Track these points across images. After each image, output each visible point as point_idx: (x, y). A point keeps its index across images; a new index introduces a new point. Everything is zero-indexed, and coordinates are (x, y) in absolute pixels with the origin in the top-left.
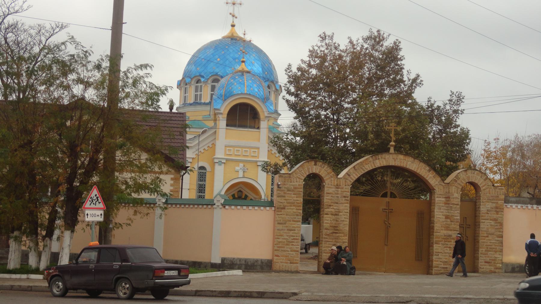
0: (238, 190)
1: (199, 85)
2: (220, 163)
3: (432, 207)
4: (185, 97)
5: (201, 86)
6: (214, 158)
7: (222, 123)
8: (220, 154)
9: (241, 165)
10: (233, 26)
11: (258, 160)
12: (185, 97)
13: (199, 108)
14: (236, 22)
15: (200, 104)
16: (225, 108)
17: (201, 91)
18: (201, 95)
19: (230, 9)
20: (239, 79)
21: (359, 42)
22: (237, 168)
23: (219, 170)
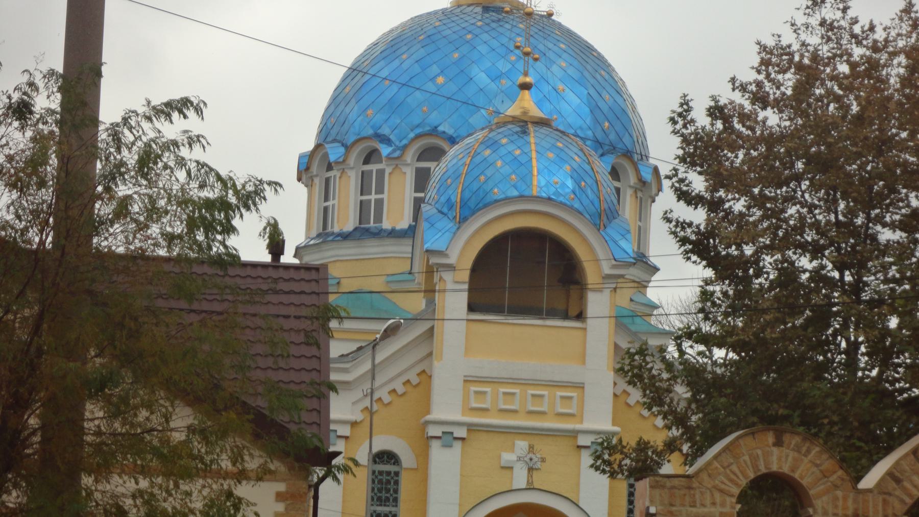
1: (373, 167)
2: (448, 439)
4: (326, 210)
5: (381, 173)
6: (428, 423)
7: (455, 301)
8: (447, 407)
11: (578, 427)
12: (326, 210)
13: (372, 248)
16: (462, 247)
17: (380, 190)
18: (379, 203)
23: (445, 463)
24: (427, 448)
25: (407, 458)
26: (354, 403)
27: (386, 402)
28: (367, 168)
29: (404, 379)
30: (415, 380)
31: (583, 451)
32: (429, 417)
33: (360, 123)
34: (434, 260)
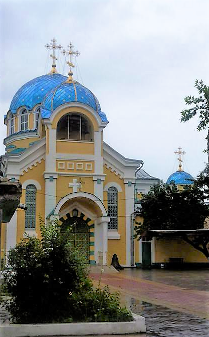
0: (74, 208)
1: (25, 114)
2: (51, 179)
3: (154, 270)
4: (12, 128)
5: (27, 116)
6: (45, 173)
7: (52, 133)
8: (51, 168)
9: (75, 180)
10: (54, 66)
11: (93, 174)
12: (12, 128)
13: (25, 136)
14: (56, 63)
15: (27, 132)
16: (54, 118)
17: (27, 120)
18: (26, 124)
19: (51, 51)
20: (68, 88)
21: (35, 236)
22: (71, 184)
23: (51, 187)
24: (45, 182)
25: (38, 187)
26: (21, 169)
27: (31, 169)
28: (23, 115)
29: (37, 161)
30: (40, 162)
31: (95, 182)
32: (7, 173)
33: (22, 101)
34: (45, 121)
